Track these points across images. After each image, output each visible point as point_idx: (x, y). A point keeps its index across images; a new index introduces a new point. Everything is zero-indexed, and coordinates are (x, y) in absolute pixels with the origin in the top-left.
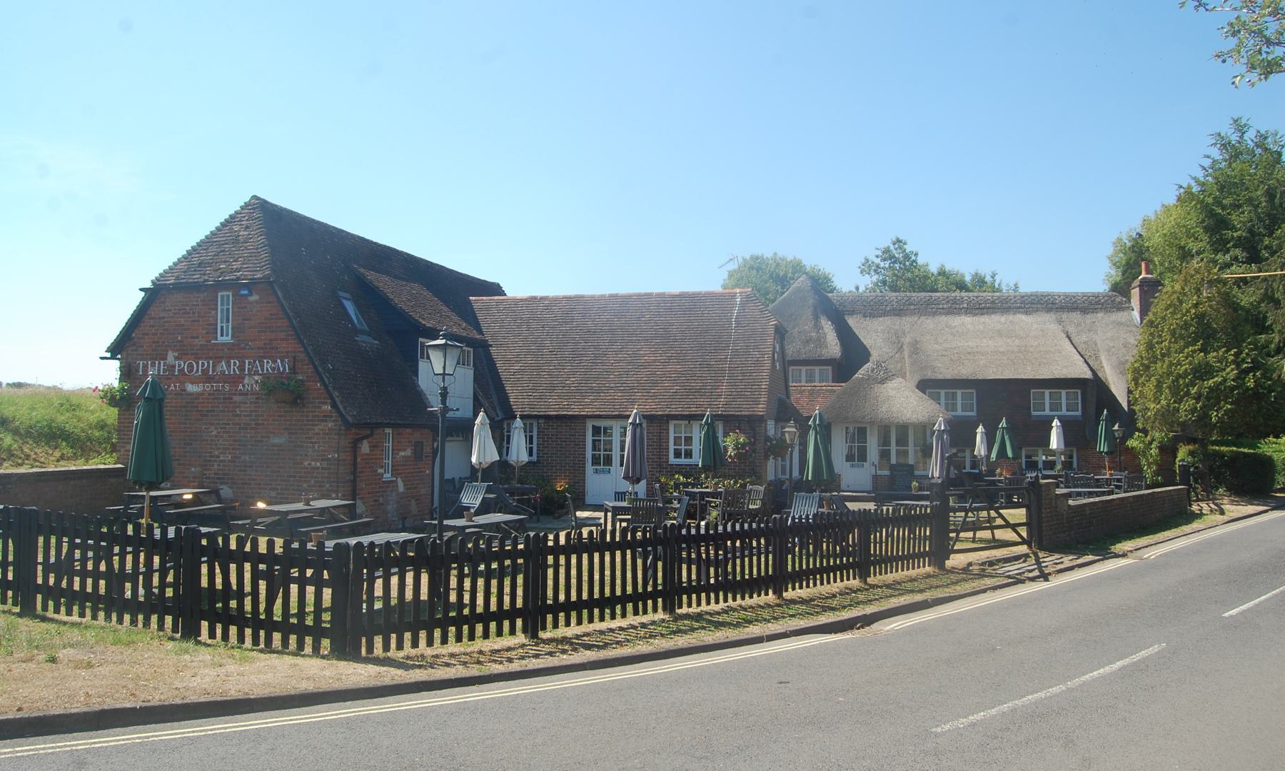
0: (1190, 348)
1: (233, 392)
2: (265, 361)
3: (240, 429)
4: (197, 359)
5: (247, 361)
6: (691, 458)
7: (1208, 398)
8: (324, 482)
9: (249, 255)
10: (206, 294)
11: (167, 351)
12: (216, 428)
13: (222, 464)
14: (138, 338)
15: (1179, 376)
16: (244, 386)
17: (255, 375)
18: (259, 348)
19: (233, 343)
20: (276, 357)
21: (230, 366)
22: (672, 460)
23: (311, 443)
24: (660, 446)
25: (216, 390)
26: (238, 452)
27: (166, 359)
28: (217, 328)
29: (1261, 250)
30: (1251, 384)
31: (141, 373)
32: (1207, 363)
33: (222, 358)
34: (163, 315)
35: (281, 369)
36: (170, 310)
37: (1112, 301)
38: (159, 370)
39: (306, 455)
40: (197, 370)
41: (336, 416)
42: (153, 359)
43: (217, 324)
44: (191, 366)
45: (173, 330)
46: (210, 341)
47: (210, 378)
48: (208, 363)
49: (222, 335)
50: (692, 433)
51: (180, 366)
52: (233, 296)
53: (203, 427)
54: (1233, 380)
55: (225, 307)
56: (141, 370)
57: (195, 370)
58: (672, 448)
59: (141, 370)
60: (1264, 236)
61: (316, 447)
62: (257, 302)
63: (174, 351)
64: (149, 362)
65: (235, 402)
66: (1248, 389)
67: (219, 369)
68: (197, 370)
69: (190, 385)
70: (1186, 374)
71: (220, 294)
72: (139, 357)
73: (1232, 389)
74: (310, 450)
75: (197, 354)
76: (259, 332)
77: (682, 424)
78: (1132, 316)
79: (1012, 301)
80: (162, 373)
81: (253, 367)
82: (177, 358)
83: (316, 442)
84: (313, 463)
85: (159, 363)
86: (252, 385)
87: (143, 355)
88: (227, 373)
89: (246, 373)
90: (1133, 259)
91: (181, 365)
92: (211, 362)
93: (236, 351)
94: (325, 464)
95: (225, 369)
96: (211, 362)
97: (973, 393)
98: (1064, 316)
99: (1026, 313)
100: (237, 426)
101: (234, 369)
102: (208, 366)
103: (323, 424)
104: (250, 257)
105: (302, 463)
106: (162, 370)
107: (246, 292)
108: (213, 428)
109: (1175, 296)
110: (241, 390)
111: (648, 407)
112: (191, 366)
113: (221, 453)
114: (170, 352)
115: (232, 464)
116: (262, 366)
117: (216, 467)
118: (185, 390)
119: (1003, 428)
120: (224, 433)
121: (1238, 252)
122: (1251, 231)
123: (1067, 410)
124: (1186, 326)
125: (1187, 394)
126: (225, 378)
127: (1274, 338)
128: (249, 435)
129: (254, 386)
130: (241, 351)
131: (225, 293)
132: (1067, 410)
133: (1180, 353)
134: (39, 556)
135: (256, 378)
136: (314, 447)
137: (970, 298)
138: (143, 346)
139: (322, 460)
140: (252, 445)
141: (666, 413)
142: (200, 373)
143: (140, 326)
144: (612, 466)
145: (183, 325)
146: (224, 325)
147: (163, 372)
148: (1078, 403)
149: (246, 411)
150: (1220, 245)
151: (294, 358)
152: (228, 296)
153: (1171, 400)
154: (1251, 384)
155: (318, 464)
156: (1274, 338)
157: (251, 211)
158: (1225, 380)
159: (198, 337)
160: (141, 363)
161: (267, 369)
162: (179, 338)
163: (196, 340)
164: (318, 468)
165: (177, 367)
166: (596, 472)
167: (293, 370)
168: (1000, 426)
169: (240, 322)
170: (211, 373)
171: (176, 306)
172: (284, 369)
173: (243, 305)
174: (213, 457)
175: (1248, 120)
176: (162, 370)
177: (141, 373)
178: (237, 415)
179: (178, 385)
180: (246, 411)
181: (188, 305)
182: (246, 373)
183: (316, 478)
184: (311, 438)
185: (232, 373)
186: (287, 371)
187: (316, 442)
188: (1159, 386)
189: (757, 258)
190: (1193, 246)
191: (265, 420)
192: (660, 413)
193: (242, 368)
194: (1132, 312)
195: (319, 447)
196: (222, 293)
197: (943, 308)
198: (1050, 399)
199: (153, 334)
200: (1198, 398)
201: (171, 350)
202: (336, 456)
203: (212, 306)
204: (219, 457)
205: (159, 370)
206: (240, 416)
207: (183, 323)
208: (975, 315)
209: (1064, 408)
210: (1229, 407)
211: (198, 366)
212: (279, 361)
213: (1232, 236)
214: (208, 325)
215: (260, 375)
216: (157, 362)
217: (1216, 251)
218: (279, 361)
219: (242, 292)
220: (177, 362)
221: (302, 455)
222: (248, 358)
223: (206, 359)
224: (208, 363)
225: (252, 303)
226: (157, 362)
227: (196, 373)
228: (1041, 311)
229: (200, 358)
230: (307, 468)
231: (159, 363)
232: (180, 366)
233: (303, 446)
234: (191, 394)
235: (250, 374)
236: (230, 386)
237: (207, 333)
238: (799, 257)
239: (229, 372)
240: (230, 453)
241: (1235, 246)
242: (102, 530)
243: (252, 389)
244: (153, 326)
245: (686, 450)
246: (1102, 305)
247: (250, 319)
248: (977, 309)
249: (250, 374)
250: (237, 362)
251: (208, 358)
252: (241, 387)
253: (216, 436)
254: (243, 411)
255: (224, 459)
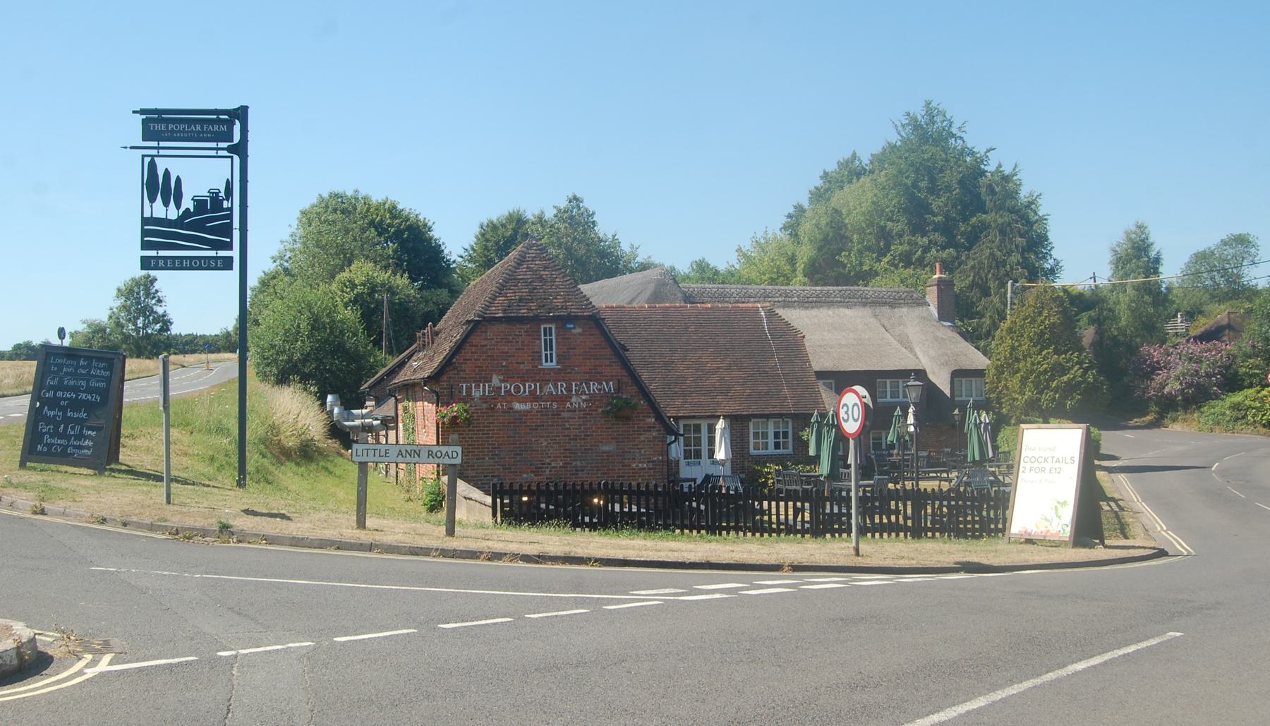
0: (1046, 351)
1: (562, 409)
2: (591, 383)
3: (569, 439)
4: (524, 382)
5: (574, 384)
6: (767, 449)
7: (1064, 390)
8: (650, 479)
9: (565, 293)
10: (529, 326)
11: (492, 374)
12: (546, 440)
13: (553, 470)
14: (459, 364)
15: (1041, 373)
16: (571, 404)
17: (582, 394)
18: (584, 373)
19: (559, 369)
20: (602, 380)
21: (557, 387)
22: (752, 451)
23: (638, 449)
24: (743, 440)
25: (544, 408)
26: (569, 459)
27: (491, 382)
28: (541, 356)
29: (957, 235)
30: (1091, 380)
31: (464, 394)
32: (1060, 364)
33: (549, 380)
34: (484, 343)
35: (607, 390)
36: (493, 339)
37: (911, 297)
38: (484, 391)
39: (633, 459)
40: (525, 391)
41: (659, 427)
42: (478, 382)
43: (541, 352)
44: (517, 388)
45: (497, 356)
46: (537, 367)
47: (537, 398)
48: (535, 385)
49: (546, 361)
50: (767, 429)
51: (506, 387)
52: (556, 328)
53: (533, 439)
54: (1080, 376)
55: (548, 338)
56: (464, 392)
57: (522, 391)
58: (752, 441)
59: (464, 392)
60: (958, 221)
61: (643, 452)
62: (580, 334)
63: (498, 374)
64: (473, 385)
65: (564, 418)
66: (1089, 383)
67: (546, 390)
68: (525, 391)
69: (518, 404)
70: (1046, 371)
71: (542, 327)
72: (462, 380)
73: (1080, 383)
74: (637, 455)
75: (523, 377)
76: (584, 359)
77: (758, 422)
78: (929, 311)
79: (833, 296)
80: (487, 394)
81: (580, 388)
82: (501, 381)
83: (642, 448)
84: (640, 465)
85: (484, 385)
86: (579, 404)
87: (465, 378)
88: (554, 393)
89: (574, 393)
90: (831, 234)
91: (507, 387)
92: (538, 384)
93: (563, 375)
94: (651, 465)
95: (553, 389)
96: (538, 384)
97: (831, 383)
98: (878, 310)
99: (848, 307)
100: (567, 438)
101: (561, 390)
102: (536, 387)
103: (648, 433)
104: (568, 295)
105: (630, 466)
106: (487, 392)
107: (572, 326)
108: (542, 440)
109: (1032, 309)
110: (568, 407)
111: (732, 408)
112: (517, 388)
113: (553, 461)
114: (494, 376)
115: (564, 469)
116: (589, 388)
117: (548, 472)
118: (512, 409)
119: (898, 415)
120: (554, 443)
121: (936, 236)
122: (947, 217)
123: (891, 398)
124: (1042, 334)
125: (1047, 387)
126: (553, 398)
127: (984, 323)
128: (578, 445)
129: (582, 404)
130: (568, 375)
131: (548, 326)
132: (891, 398)
133: (1037, 355)
134: (792, 516)
135: (584, 397)
136: (640, 452)
137: (797, 291)
138: (465, 371)
139: (648, 462)
140: (582, 453)
141: (750, 413)
142: (527, 394)
143: (461, 353)
144: (701, 458)
145: (507, 353)
146: (548, 353)
147: (489, 393)
148: (886, 391)
149: (575, 425)
150: (918, 228)
151: (619, 381)
152: (550, 329)
153: (1033, 392)
154: (1091, 380)
155: (645, 465)
156: (984, 323)
157: (538, 252)
158: (1074, 377)
159: (523, 363)
160: (464, 385)
161: (594, 390)
162: (504, 364)
163: (522, 365)
164: (645, 469)
165: (503, 388)
166: (688, 464)
167: (619, 389)
168: (896, 414)
169: (565, 350)
170: (538, 393)
171: (498, 335)
172: (610, 390)
173: (567, 336)
174: (545, 464)
175: (938, 105)
176: (487, 392)
177: (464, 394)
178: (568, 429)
179: (504, 404)
180: (575, 425)
181: (510, 335)
182: (574, 393)
183: (643, 476)
184: (637, 445)
185: (559, 393)
186: (613, 391)
187: (642, 448)
188: (1024, 380)
189: (337, 196)
190: (895, 227)
191: (594, 431)
192: (745, 413)
193: (569, 389)
194: (930, 308)
195: (645, 452)
196: (545, 326)
197: (779, 302)
198: (898, 391)
199: (476, 360)
200: (1056, 390)
201: (496, 374)
202: (661, 458)
203: (536, 337)
204: (550, 464)
205: (484, 391)
206: (569, 429)
207: (506, 350)
208: (807, 308)
209: (889, 396)
210: (1079, 397)
211: (525, 388)
212: (604, 383)
213: (934, 221)
214: (533, 352)
215: (587, 394)
216: (481, 385)
217: (913, 233)
218: (604, 383)
219: (568, 326)
220: (503, 385)
221: (629, 459)
222: (574, 381)
223: (532, 381)
224: (535, 385)
225: (575, 335)
226: (481, 385)
227: (523, 393)
228: (859, 305)
229: (527, 381)
230: (635, 469)
231: (484, 385)
232: (506, 387)
233: (630, 452)
234: (517, 412)
235: (577, 394)
236: (557, 405)
237: (532, 360)
238: (393, 198)
239: (557, 393)
240: (561, 460)
241: (935, 230)
242: (642, 518)
243: (579, 407)
244: (475, 353)
245: (783, 442)
246: (904, 300)
247: (575, 349)
248: (806, 302)
249: (577, 394)
250: (564, 384)
251: (535, 381)
252: (568, 405)
253: (546, 447)
254: (572, 425)
255: (555, 465)
